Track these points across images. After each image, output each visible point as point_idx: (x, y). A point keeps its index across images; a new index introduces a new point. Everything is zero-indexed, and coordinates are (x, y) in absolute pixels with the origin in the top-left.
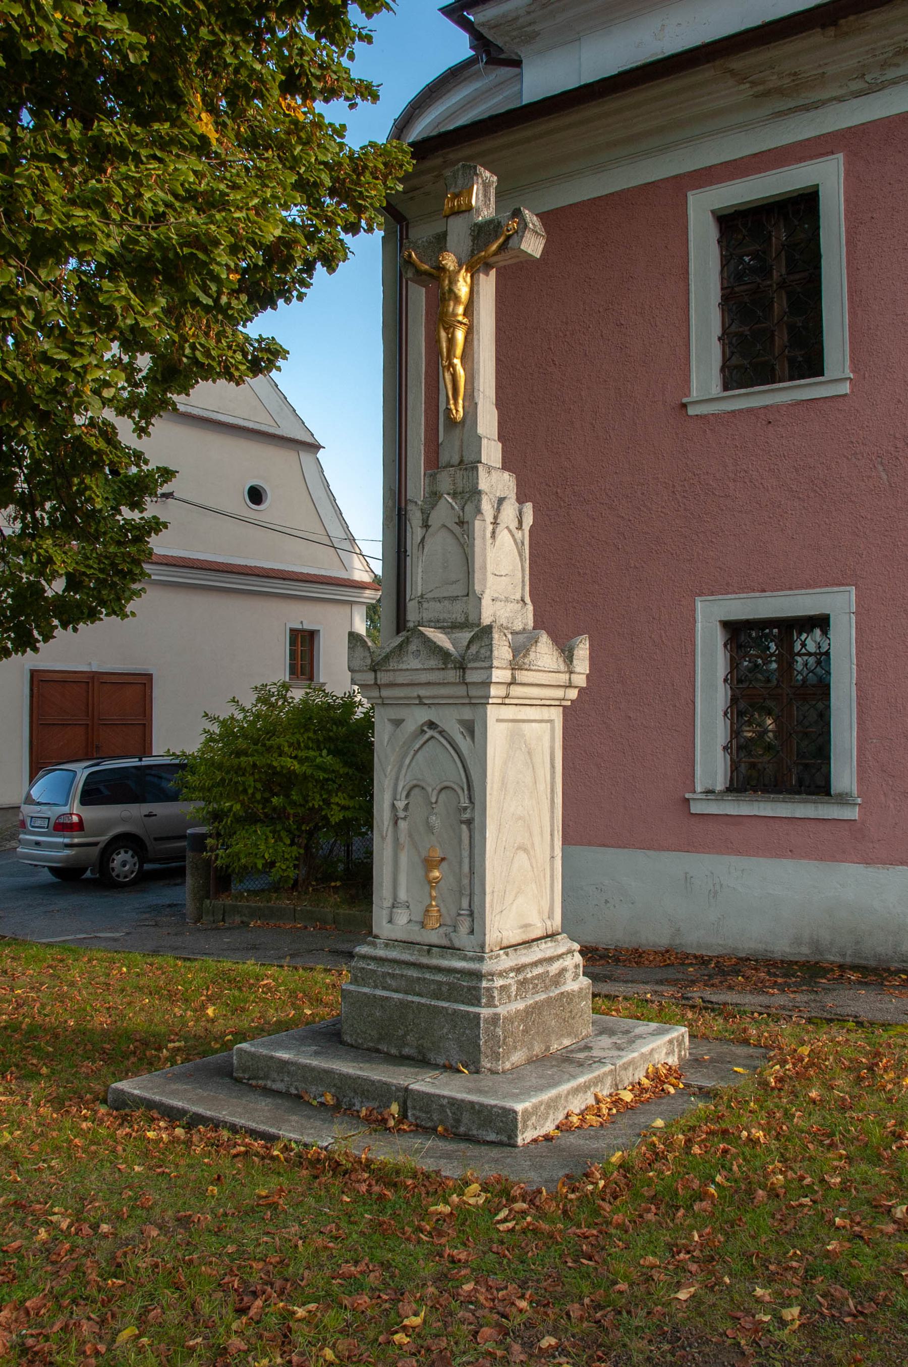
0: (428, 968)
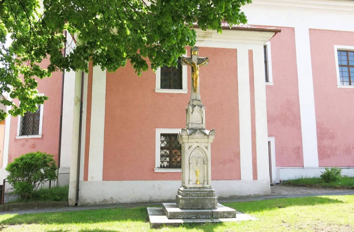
0: (202, 191)
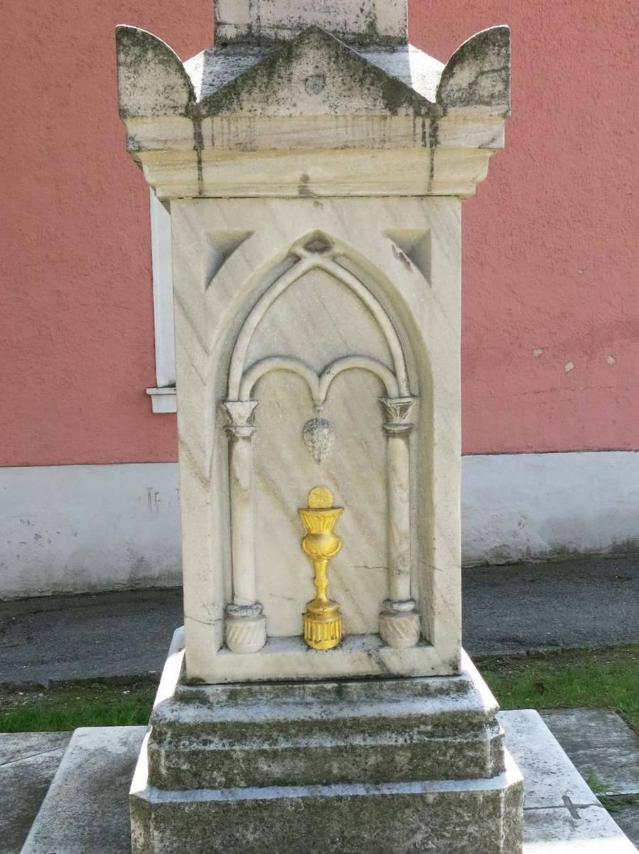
0: (358, 726)
